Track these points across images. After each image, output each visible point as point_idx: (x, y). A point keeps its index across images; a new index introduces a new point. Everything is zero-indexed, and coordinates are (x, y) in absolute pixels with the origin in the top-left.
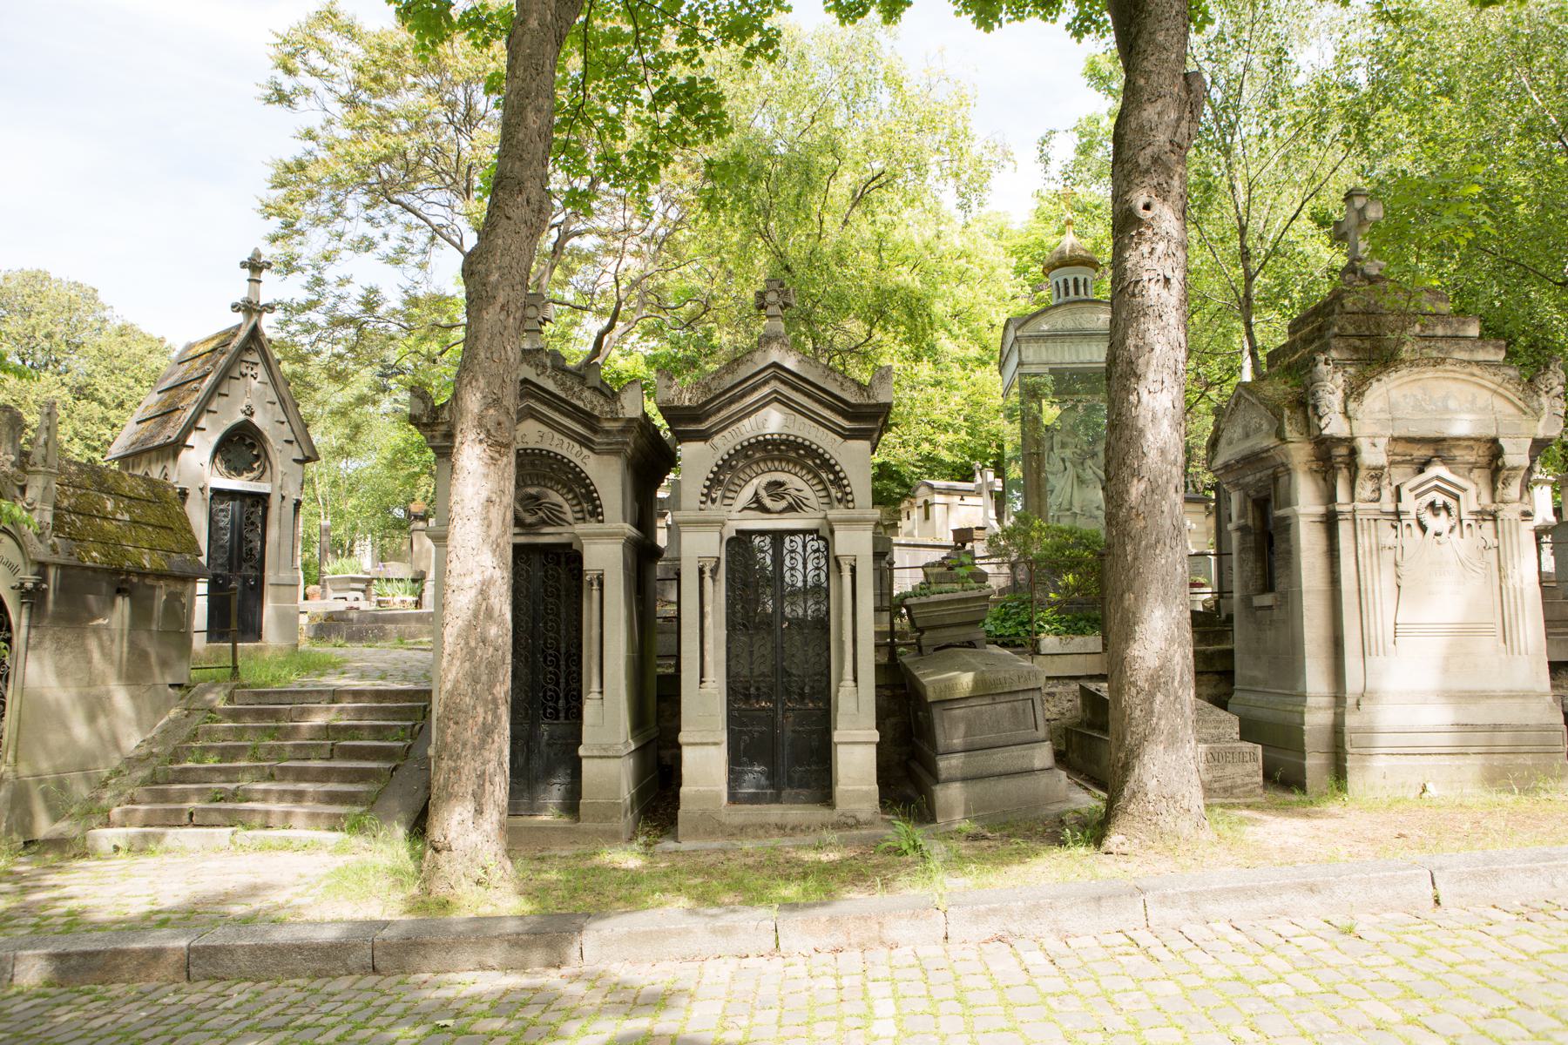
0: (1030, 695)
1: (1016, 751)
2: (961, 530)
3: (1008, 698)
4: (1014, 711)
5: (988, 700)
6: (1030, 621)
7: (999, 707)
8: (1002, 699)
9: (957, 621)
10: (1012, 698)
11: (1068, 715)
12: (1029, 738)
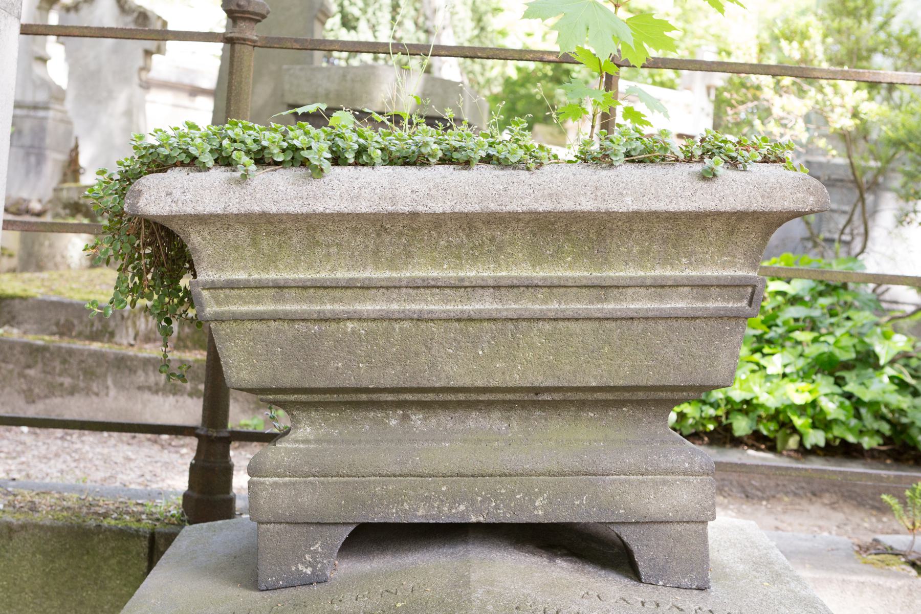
9: (523, 369)
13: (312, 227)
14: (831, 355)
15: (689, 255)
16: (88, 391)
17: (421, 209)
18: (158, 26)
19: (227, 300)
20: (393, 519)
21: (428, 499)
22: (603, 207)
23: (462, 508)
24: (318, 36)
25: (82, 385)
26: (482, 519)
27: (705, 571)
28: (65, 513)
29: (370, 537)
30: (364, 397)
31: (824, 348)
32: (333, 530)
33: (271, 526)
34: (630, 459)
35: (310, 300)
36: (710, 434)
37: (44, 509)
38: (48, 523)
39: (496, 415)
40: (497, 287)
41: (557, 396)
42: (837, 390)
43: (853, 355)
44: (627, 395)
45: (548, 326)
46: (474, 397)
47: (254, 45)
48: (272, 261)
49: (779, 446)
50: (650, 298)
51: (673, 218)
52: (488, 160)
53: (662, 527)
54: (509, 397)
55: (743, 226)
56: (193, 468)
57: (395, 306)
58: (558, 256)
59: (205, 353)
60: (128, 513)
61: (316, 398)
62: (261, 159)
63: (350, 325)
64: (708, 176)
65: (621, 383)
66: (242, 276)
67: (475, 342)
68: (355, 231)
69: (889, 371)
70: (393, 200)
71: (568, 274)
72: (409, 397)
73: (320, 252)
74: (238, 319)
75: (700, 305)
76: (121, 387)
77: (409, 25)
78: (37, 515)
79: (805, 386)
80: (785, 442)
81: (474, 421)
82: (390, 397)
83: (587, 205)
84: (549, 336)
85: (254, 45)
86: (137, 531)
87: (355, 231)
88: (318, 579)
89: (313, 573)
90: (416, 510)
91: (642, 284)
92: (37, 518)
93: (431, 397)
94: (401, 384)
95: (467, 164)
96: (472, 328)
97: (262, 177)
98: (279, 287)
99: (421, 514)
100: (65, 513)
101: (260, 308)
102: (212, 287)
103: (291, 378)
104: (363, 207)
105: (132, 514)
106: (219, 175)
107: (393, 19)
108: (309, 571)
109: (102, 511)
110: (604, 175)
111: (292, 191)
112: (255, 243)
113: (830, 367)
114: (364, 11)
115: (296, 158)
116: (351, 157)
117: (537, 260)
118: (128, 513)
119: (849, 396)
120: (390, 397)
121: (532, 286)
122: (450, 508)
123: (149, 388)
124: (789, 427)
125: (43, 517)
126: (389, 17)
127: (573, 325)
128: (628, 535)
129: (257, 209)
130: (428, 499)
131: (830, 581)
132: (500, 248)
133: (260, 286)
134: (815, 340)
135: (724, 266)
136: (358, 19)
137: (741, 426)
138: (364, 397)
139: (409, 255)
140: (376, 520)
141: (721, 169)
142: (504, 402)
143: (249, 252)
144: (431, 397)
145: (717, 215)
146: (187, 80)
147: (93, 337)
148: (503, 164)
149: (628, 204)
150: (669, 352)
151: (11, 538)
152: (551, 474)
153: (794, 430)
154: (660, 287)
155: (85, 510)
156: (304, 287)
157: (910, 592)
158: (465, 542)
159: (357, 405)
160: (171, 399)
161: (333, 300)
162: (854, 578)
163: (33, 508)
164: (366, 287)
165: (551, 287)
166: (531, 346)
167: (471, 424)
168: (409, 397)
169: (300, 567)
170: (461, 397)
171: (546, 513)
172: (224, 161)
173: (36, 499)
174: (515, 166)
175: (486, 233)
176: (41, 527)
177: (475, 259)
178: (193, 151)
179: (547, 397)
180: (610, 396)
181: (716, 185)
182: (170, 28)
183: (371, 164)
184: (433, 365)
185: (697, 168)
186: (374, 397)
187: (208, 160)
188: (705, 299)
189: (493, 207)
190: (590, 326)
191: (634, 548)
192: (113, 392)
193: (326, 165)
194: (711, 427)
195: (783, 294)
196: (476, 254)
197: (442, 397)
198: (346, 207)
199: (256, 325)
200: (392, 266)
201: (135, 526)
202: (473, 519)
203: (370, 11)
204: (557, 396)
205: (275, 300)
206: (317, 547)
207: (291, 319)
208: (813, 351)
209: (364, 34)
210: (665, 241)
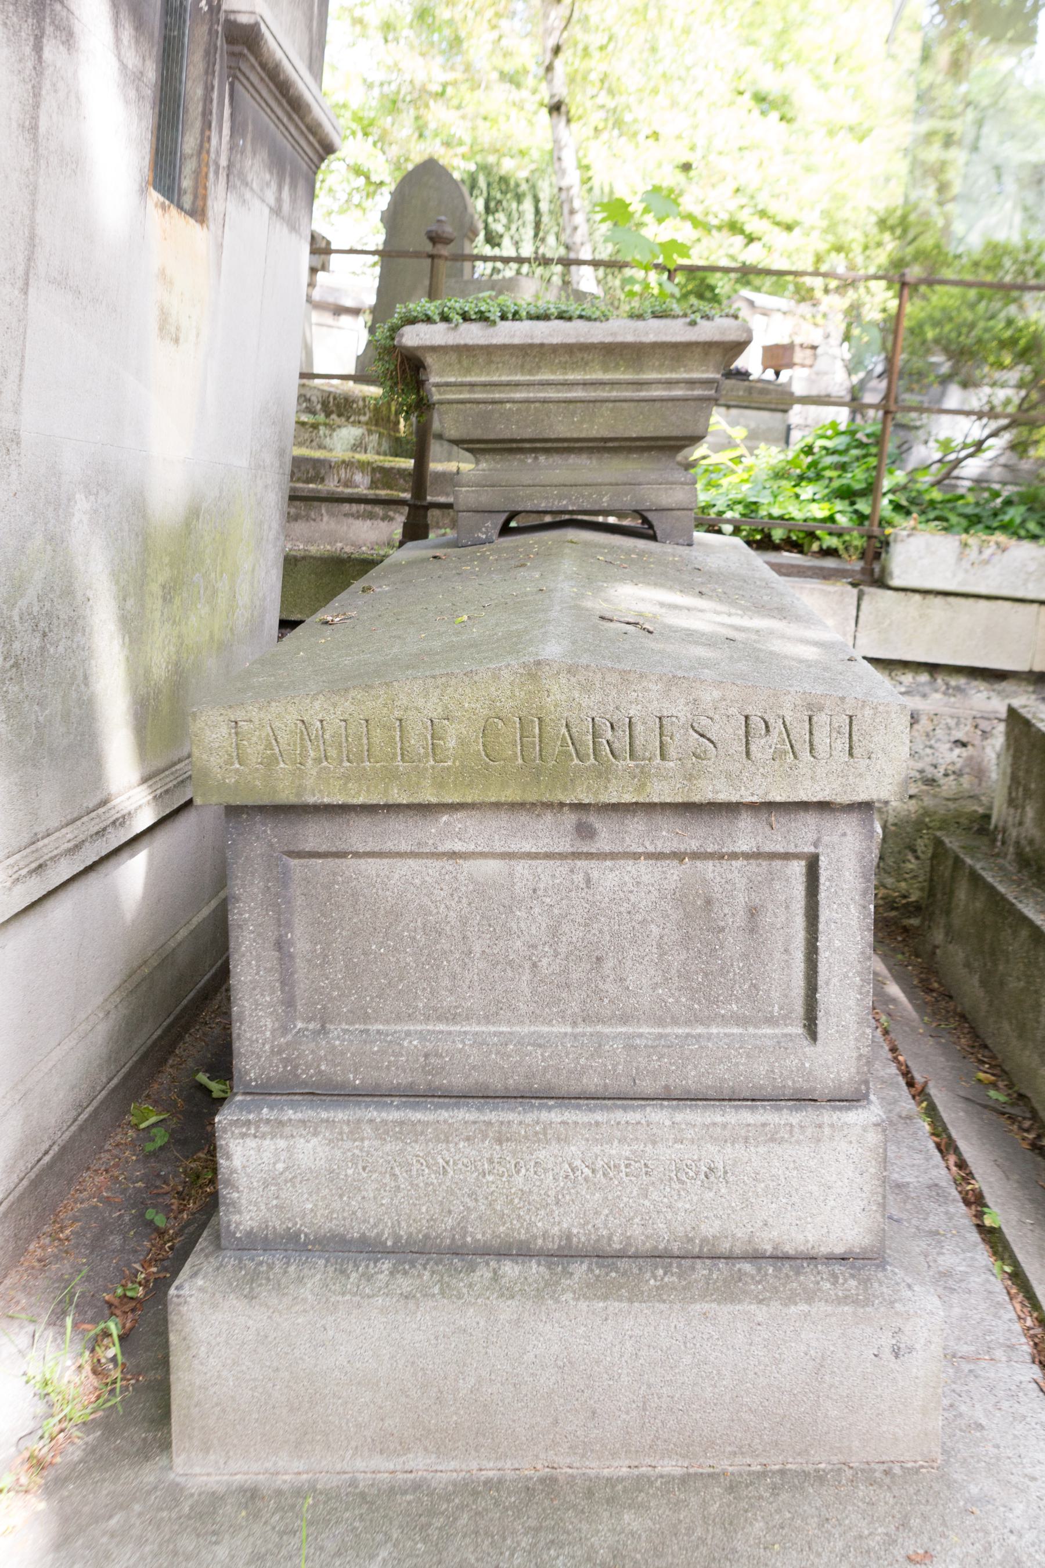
0: (801, 836)
1: (673, 1136)
2: (777, 346)
3: (669, 835)
4: (699, 910)
5: (550, 834)
6: (871, 490)
7: (609, 877)
8: (635, 834)
9: (597, 428)
10: (695, 836)
11: (949, 786)
12: (759, 1072)
13: (490, 353)
14: (849, 486)
15: (685, 366)
16: (308, 518)
17: (546, 341)
18: (323, 245)
19: (445, 393)
21: (547, 498)
22: (638, 340)
24: (467, 251)
25: (303, 513)
30: (514, 445)
31: (844, 481)
32: (497, 515)
34: (653, 476)
35: (488, 392)
36: (757, 542)
39: (584, 456)
40: (585, 384)
41: (616, 444)
42: (850, 509)
43: (863, 485)
44: (653, 443)
45: (611, 405)
46: (572, 445)
47: (446, 258)
48: (468, 371)
49: (806, 549)
50: (665, 389)
51: (675, 346)
52: (581, 317)
54: (591, 444)
55: (712, 351)
56: (405, 524)
57: (531, 395)
58: (617, 367)
59: (412, 461)
61: (490, 446)
62: (465, 317)
63: (508, 406)
64: (693, 323)
65: (649, 435)
66: (452, 379)
67: (573, 414)
68: (512, 355)
69: (890, 496)
70: (532, 337)
71: (622, 377)
72: (538, 445)
73: (494, 366)
74: (451, 402)
75: (690, 393)
76: (332, 514)
77: (551, 240)
79: (826, 505)
80: (810, 546)
81: (573, 459)
82: (528, 445)
83: (630, 338)
84: (612, 410)
85: (446, 258)
87: (512, 355)
91: (659, 382)
93: (549, 445)
94: (534, 436)
95: (570, 319)
96: (571, 406)
97: (465, 327)
98: (472, 385)
101: (462, 396)
102: (437, 385)
103: (477, 434)
104: (516, 341)
106: (443, 326)
107: (536, 235)
110: (640, 324)
111: (480, 333)
112: (460, 362)
113: (848, 494)
114: (508, 228)
115: (482, 317)
116: (510, 316)
117: (606, 370)
119: (856, 512)
120: (528, 445)
121: (602, 383)
123: (352, 515)
124: (812, 535)
126: (531, 233)
127: (625, 405)
129: (462, 342)
130: (547, 498)
132: (586, 364)
133: (462, 385)
134: (839, 476)
135: (703, 372)
136: (501, 236)
137: (778, 535)
138: (514, 445)
139: (540, 368)
141: (698, 320)
142: (588, 448)
143: (457, 367)
144: (549, 445)
145: (697, 344)
146: (331, 300)
147: (308, 481)
148: (589, 319)
149: (651, 338)
150: (674, 418)
152: (611, 484)
153: (818, 539)
154: (670, 383)
156: (484, 385)
157: (842, 594)
159: (511, 451)
160: (368, 522)
161: (500, 392)
164: (517, 385)
165: (613, 384)
166: (602, 416)
167: (571, 461)
168: (538, 445)
170: (566, 445)
172: (445, 318)
174: (595, 320)
175: (579, 355)
177: (573, 370)
178: (429, 313)
179: (610, 444)
180: (643, 444)
181: (696, 328)
182: (333, 247)
183: (520, 319)
184: (551, 426)
185: (688, 320)
186: (520, 445)
187: (437, 318)
188: (693, 389)
189: (582, 340)
190: (632, 404)
192: (326, 518)
193: (498, 320)
194: (758, 537)
195: (825, 448)
196: (575, 366)
197: (555, 445)
198: (507, 341)
199: (460, 406)
200: (530, 373)
203: (514, 227)
204: (616, 444)
205: (470, 392)
206: (489, 524)
207: (477, 402)
208: (836, 484)
209: (507, 249)
210: (672, 359)
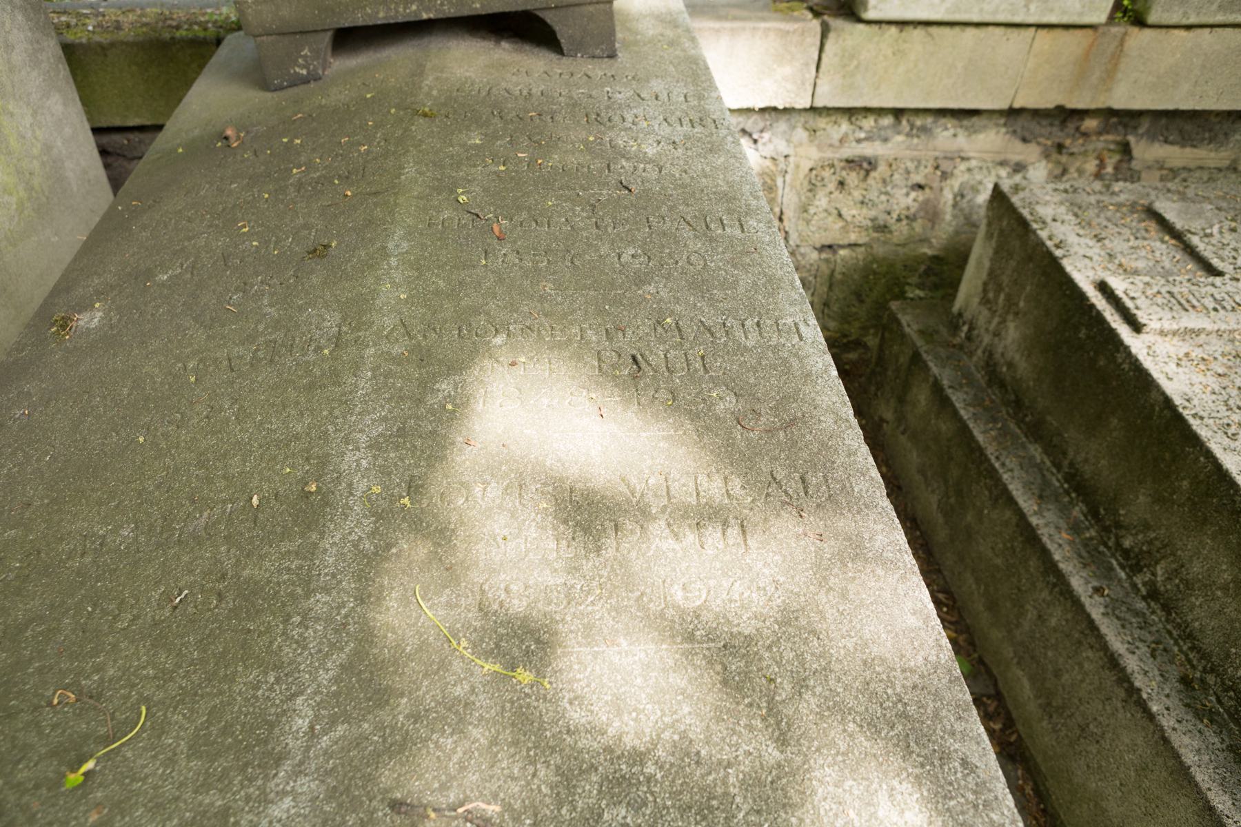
20: (360, 23)
23: (414, 7)
26: (432, 16)
27: (613, 43)
28: (144, 29)
29: (349, 38)
33: (264, 38)
37: (126, 26)
38: (131, 39)
53: (577, 9)
60: (196, 23)
78: (121, 33)
86: (205, 38)
88: (312, 78)
89: (308, 73)
90: (377, 13)
92: (121, 36)
99: (382, 16)
100: (144, 29)
105: (200, 24)
108: (304, 72)
109: (174, 23)
118: (196, 23)
122: (405, 9)
125: (127, 34)
128: (549, 17)
131: (744, 29)
140: (347, 25)
151: (105, 55)
155: (160, 24)
158: (430, 33)
162: (763, 25)
163: (118, 26)
169: (297, 69)
171: (483, 6)
173: (121, 18)
176: (127, 44)
191: (557, 28)
201: (201, 34)
202: (425, 16)
206: (306, 52)
